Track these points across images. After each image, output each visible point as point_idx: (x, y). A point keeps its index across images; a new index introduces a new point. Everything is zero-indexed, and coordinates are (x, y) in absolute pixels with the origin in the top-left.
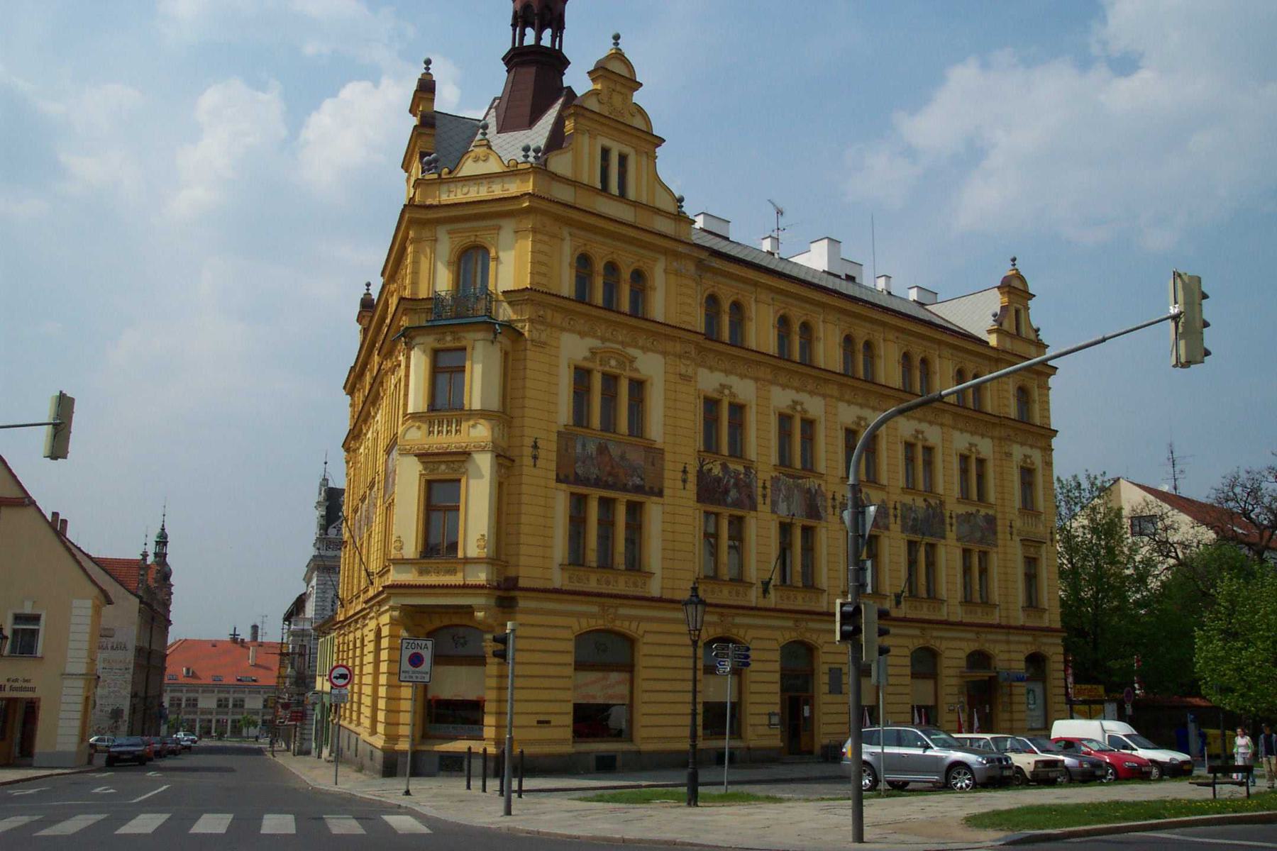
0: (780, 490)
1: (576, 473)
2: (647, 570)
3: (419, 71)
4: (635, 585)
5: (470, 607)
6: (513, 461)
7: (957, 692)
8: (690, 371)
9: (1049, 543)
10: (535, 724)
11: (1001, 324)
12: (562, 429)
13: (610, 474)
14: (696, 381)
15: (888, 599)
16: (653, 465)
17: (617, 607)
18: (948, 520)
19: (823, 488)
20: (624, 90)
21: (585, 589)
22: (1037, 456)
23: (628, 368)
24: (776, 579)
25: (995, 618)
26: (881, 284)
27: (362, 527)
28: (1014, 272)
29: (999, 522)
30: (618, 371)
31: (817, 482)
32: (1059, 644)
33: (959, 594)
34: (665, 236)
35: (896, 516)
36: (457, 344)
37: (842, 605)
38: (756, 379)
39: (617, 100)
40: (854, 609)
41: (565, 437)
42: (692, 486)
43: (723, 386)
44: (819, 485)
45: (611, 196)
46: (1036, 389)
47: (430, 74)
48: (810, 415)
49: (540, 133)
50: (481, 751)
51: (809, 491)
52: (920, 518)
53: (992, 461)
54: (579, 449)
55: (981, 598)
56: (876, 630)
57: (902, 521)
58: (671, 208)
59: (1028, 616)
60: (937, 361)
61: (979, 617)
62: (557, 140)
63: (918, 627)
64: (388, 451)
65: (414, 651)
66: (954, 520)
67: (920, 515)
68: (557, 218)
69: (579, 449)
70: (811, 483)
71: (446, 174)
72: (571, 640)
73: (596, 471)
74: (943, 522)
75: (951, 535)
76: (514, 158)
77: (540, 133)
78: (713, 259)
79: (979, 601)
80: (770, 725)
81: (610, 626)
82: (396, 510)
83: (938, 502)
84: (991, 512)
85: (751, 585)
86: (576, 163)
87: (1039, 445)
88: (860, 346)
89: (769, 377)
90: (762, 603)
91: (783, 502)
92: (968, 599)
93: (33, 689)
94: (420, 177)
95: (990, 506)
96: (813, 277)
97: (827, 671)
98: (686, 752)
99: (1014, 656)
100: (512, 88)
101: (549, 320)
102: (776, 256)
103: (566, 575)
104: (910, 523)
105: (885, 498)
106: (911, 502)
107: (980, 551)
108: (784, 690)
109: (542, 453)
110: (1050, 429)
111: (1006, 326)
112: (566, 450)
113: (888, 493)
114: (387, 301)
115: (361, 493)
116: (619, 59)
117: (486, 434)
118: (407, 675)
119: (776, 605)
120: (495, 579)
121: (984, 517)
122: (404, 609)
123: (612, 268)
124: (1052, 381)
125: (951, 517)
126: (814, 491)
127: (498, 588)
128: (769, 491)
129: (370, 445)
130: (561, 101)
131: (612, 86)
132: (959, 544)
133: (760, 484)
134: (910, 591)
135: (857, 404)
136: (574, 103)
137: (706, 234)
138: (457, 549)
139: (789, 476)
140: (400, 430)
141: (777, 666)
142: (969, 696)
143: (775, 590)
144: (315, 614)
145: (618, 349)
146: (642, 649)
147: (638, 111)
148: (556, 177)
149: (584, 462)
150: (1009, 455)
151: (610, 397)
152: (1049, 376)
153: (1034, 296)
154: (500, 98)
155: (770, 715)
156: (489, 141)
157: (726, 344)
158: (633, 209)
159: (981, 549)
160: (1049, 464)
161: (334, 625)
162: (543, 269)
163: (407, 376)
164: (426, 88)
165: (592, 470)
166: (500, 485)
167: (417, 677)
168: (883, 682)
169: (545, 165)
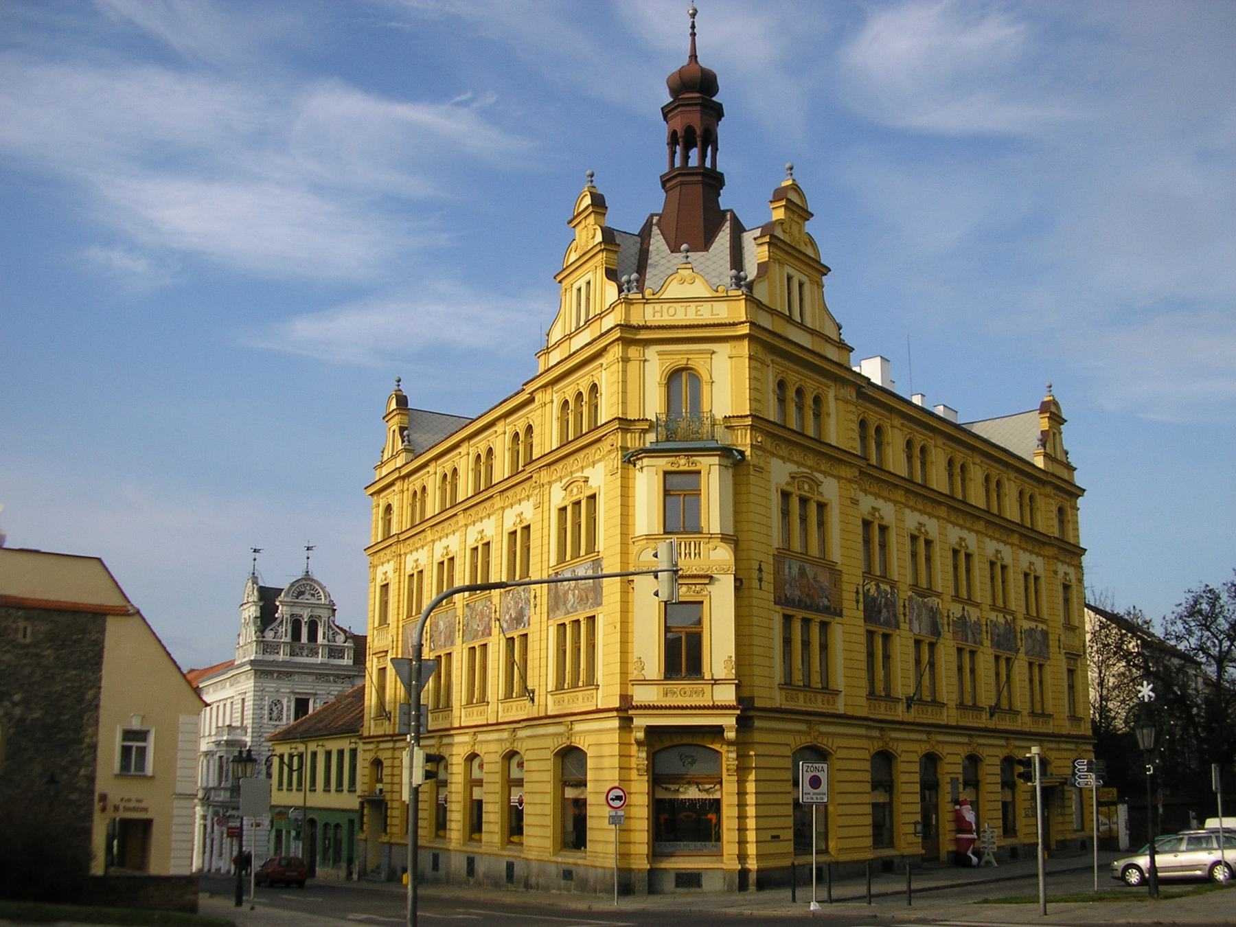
0: (914, 609)
2: (1048, 713)
10: (769, 838)
13: (808, 595)
18: (1019, 635)
22: (1071, 571)
25: (1049, 729)
28: (1051, 398)
29: (1051, 637)
30: (809, 495)
31: (937, 600)
32: (1089, 751)
35: (987, 632)
36: (692, 468)
39: (795, 228)
46: (1069, 510)
48: (930, 537)
63: (1074, 742)
65: (813, 774)
71: (649, 295)
74: (1015, 636)
80: (915, 833)
84: (1045, 627)
89: (903, 500)
93: (145, 810)
95: (1044, 621)
97: (949, 780)
103: (783, 693)
110: (1079, 547)
112: (778, 573)
116: (795, 189)
117: (728, 558)
118: (809, 796)
119: (781, 704)
122: (650, 730)
124: (1080, 502)
125: (1021, 632)
130: (728, 224)
135: (996, 539)
141: (917, 778)
145: (807, 473)
149: (791, 586)
150: (1055, 572)
153: (1066, 421)
155: (915, 823)
158: (810, 336)
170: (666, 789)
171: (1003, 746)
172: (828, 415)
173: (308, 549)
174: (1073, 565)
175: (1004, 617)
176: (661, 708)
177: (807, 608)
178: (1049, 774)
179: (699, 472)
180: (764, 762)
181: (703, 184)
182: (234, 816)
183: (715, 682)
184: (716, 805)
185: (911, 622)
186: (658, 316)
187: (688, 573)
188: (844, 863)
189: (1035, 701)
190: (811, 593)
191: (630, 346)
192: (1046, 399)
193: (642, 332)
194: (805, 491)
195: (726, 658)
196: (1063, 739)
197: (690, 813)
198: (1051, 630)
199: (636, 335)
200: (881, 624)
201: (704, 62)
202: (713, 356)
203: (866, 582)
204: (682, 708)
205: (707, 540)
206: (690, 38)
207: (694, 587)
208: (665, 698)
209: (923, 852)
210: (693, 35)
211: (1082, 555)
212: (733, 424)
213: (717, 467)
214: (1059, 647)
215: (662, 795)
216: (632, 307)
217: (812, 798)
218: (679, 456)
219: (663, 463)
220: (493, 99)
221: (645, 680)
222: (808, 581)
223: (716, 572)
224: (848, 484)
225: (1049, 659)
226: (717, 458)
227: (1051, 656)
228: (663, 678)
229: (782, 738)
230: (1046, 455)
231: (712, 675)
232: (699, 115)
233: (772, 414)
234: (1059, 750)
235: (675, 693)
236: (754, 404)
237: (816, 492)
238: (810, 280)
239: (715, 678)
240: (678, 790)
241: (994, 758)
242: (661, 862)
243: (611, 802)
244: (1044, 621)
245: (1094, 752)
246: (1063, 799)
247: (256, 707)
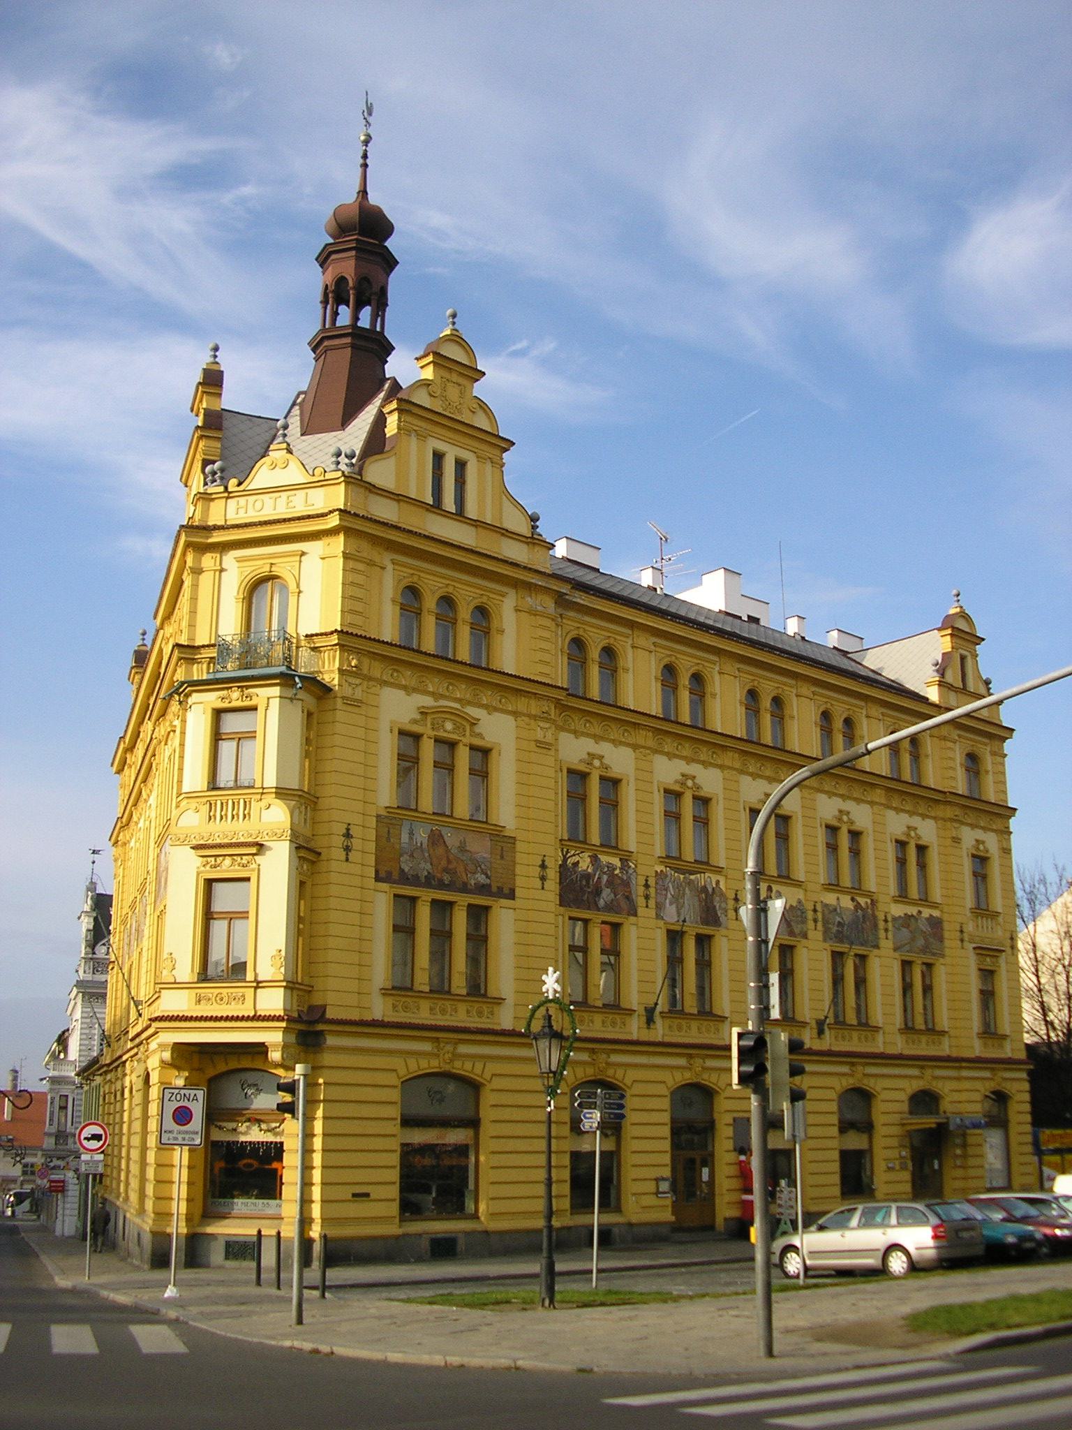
1: (402, 871)
2: (875, 1024)
3: (205, 359)
4: (480, 1014)
5: (263, 1044)
6: (319, 854)
7: (897, 1144)
8: (549, 738)
9: (1008, 950)
10: (350, 1197)
11: (943, 675)
12: (383, 813)
13: (446, 870)
14: (557, 750)
15: (808, 1028)
16: (502, 857)
17: (456, 1044)
18: (881, 925)
19: (722, 886)
20: (461, 380)
21: (413, 1021)
22: (991, 842)
23: (468, 733)
24: (663, 1006)
25: (945, 1048)
26: (792, 627)
27: (132, 942)
29: (946, 926)
30: (455, 737)
31: (714, 878)
33: (898, 1020)
34: (515, 565)
35: (815, 921)
36: (247, 703)
37: (740, 1036)
38: (635, 747)
39: (453, 393)
40: (755, 1042)
41: (388, 823)
42: (553, 885)
43: (592, 756)
44: (718, 882)
45: (447, 514)
47: (217, 363)
49: (356, 434)
50: (274, 1232)
51: (704, 889)
52: (847, 923)
53: (721, 802)
54: (405, 837)
55: (926, 1022)
56: (787, 1067)
57: (824, 925)
58: (524, 529)
59: (985, 1045)
60: (865, 721)
61: (924, 1047)
62: (376, 443)
64: (160, 841)
65: (181, 1104)
66: (890, 924)
67: (847, 918)
68: (375, 541)
69: (405, 837)
70: (706, 879)
71: (234, 487)
72: (395, 1087)
73: (428, 866)
74: (876, 926)
75: (887, 944)
76: (322, 465)
77: (356, 434)
78: (577, 594)
79: (923, 1027)
80: (657, 1193)
81: (447, 1068)
82: (169, 919)
83: (869, 901)
84: (936, 913)
85: (631, 1012)
86: (401, 474)
87: (994, 827)
88: (594, 653)
89: (737, 765)
90: (646, 1035)
91: (671, 904)
92: (910, 1024)
94: (202, 490)
95: (934, 906)
96: (698, 613)
97: (731, 1122)
98: (539, 1231)
99: (964, 1096)
100: (321, 381)
101: (365, 672)
102: (659, 592)
103: (390, 1001)
104: (835, 929)
105: (802, 897)
106: (834, 902)
107: (924, 963)
108: (676, 1146)
109: (356, 843)
111: (949, 677)
112: (388, 839)
113: (806, 890)
114: (161, 650)
115: (131, 898)
118: (171, 1136)
120: (295, 1008)
121: (927, 919)
122: (178, 1048)
123: (447, 602)
124: (1008, 746)
125: (886, 921)
126: (710, 890)
127: (299, 1020)
128: (652, 891)
129: (141, 837)
130: (384, 393)
131: (446, 375)
132: (897, 955)
133: (642, 881)
134: (836, 1016)
136: (399, 396)
137: (569, 564)
138: (245, 969)
139: (677, 870)
140: (175, 813)
141: (666, 1117)
142: (913, 1149)
143: (663, 1017)
144: (80, 1056)
146: (488, 1098)
147: (481, 406)
148: (372, 489)
149: (412, 856)
150: (957, 840)
151: (445, 767)
152: (1004, 739)
153: (983, 639)
154: (304, 393)
155: (658, 1180)
156: (288, 445)
157: (687, 726)
158: (473, 529)
159: (925, 961)
160: (1007, 851)
161: (99, 1069)
162: (359, 607)
163: (182, 745)
164: (212, 380)
165: (423, 865)
166: (302, 884)
167: (184, 1139)
168: (800, 1134)
169: (360, 474)
170: (220, 1128)
171: (916, 1077)
172: (502, 632)
173: (94, 852)
174: (993, 830)
175: (853, 899)
176: (191, 1019)
177: (441, 886)
178: (941, 1112)
179: (255, 709)
180: (337, 1093)
181: (352, 347)
182: (60, 1167)
183: (258, 985)
184: (276, 1151)
185: (659, 907)
186: (242, 513)
187: (210, 842)
188: (501, 1233)
189: (916, 1012)
190: (450, 867)
191: (204, 554)
192: (952, 611)
193: (215, 533)
194: (445, 731)
195: (275, 953)
196: (964, 1064)
197: (249, 1161)
198: (945, 917)
199: (208, 538)
200: (598, 909)
201: (374, 199)
202: (303, 558)
203: (565, 850)
204: (217, 1019)
205: (259, 797)
206: (359, 171)
207: (239, 858)
208: (198, 1007)
209: (673, 1218)
210: (365, 166)
211: (1010, 817)
212: (317, 645)
213: (278, 699)
214: (962, 940)
215: (217, 1136)
216: (212, 504)
217: (176, 1139)
218: (231, 688)
219: (212, 699)
220: (552, 346)
221: (175, 983)
222: (448, 851)
223: (267, 838)
224: (532, 722)
225: (943, 956)
226: (278, 688)
227: (947, 952)
228: (196, 980)
229: (379, 1062)
230: (941, 684)
231: (256, 975)
232: (352, 262)
233: (388, 627)
234: (958, 1079)
235: (209, 999)
236: (349, 618)
237: (468, 733)
238: (478, 457)
239: (260, 978)
240: (235, 1130)
241: (829, 1091)
242: (208, 1225)
243: (85, 1143)
244: (934, 906)
245: (1029, 1081)
246: (964, 1146)
247: (84, 1037)
